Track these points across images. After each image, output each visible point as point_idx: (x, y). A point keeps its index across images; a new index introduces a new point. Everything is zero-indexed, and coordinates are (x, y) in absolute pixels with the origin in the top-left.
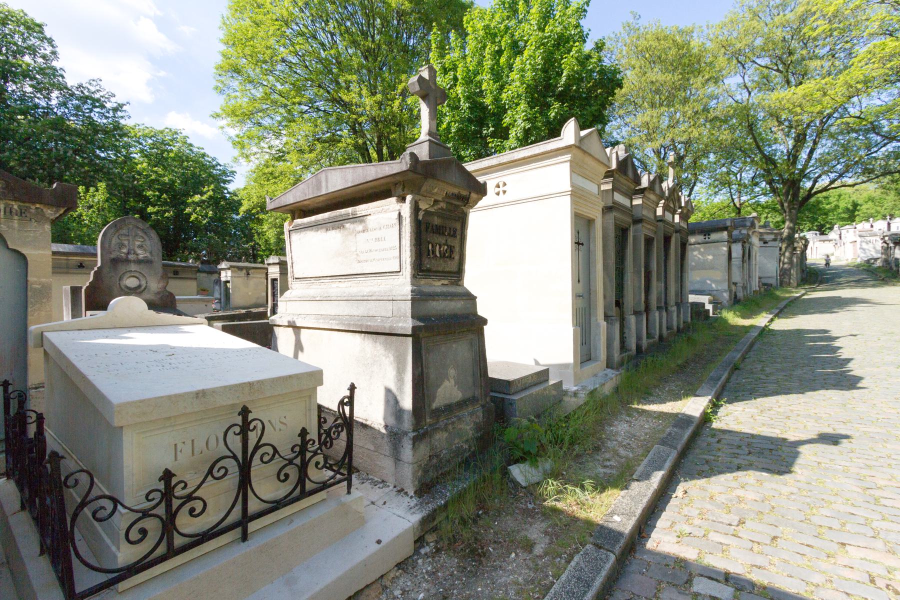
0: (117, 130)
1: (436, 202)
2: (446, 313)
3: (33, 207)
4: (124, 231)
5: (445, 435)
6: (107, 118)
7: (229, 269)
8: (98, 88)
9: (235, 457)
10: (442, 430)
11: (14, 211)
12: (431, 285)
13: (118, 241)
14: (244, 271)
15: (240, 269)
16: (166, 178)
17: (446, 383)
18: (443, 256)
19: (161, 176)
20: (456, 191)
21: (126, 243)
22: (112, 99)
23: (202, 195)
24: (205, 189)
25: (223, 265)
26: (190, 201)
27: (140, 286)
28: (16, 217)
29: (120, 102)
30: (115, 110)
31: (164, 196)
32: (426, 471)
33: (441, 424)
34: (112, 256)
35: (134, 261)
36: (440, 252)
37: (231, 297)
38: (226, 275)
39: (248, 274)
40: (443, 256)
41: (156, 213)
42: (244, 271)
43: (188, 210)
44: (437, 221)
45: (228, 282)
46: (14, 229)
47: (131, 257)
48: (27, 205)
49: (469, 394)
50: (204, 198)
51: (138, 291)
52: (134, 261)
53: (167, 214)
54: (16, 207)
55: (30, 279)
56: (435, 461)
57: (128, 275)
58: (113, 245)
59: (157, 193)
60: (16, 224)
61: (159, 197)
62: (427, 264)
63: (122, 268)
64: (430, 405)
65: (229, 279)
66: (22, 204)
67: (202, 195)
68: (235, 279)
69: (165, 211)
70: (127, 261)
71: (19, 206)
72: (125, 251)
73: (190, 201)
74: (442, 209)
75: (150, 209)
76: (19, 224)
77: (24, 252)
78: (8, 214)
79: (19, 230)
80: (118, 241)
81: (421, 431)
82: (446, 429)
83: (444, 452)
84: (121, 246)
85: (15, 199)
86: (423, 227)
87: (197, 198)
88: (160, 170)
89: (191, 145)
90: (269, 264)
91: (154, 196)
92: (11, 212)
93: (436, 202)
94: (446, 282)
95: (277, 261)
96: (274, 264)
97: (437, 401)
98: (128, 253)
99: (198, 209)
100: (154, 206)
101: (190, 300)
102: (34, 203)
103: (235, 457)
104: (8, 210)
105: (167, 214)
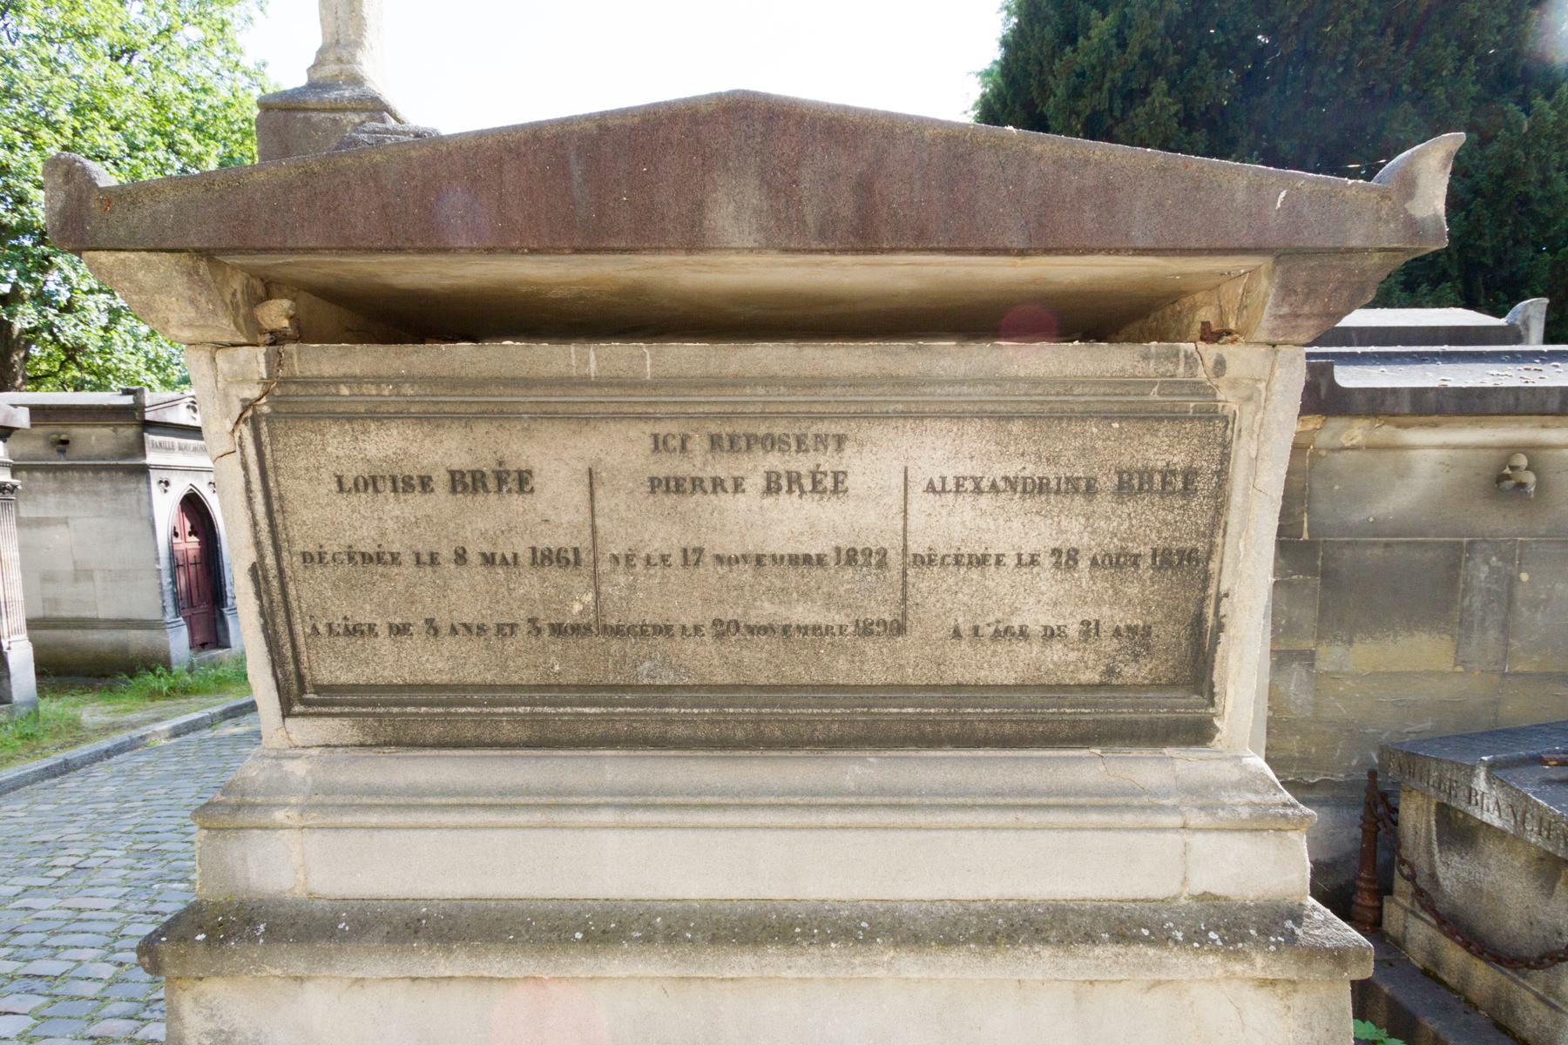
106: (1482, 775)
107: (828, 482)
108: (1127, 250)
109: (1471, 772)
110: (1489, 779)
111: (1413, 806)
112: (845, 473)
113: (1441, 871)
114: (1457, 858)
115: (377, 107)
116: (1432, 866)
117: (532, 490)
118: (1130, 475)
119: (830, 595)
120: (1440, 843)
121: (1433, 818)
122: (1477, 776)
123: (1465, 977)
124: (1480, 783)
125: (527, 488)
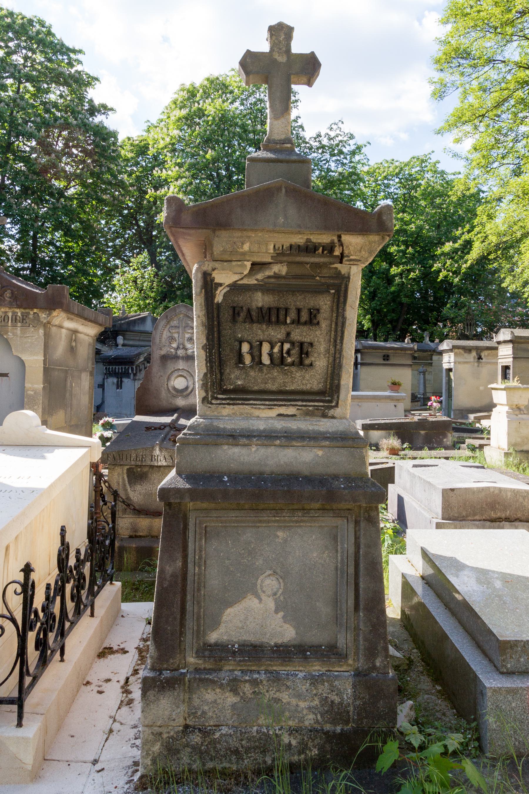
0: (353, 178)
1: (257, 266)
2: (268, 470)
3: (32, 313)
4: (175, 323)
5: (231, 699)
6: (343, 164)
7: (451, 350)
8: (338, 132)
9: (13, 620)
10: (221, 686)
11: (18, 318)
12: (249, 417)
13: (169, 334)
14: (474, 354)
15: (468, 350)
16: (413, 226)
17: (251, 602)
18: (279, 362)
19: (407, 223)
20: (299, 240)
21: (176, 335)
22: (351, 142)
23: (455, 242)
24: (458, 233)
25: (445, 345)
26: (439, 252)
27: (187, 388)
28: (19, 324)
29: (360, 143)
30: (353, 153)
31: (410, 250)
32: (171, 750)
33: (224, 676)
34: (163, 352)
35: (183, 358)
36: (271, 355)
37: (454, 393)
38: (448, 360)
39: (480, 358)
40: (279, 362)
41: (401, 274)
42: (474, 354)
43: (437, 266)
44: (260, 300)
45: (450, 370)
46: (17, 336)
47: (180, 352)
48: (27, 311)
49: (317, 637)
50: (457, 245)
51: (185, 394)
52: (183, 358)
53: (412, 275)
54: (19, 314)
55: (28, 385)
56: (196, 738)
57: (176, 374)
58: (163, 340)
59: (403, 248)
60: (18, 331)
61: (404, 252)
62: (236, 378)
63: (171, 366)
64: (199, 634)
65: (452, 366)
66: (23, 311)
67: (455, 242)
68: (460, 367)
69: (409, 271)
70: (176, 357)
71: (22, 313)
72: (174, 345)
73: (439, 252)
74: (277, 276)
75: (394, 270)
76: (21, 330)
77: (23, 359)
78: (14, 322)
79: (21, 337)
80: (169, 334)
81: (167, 674)
82: (234, 686)
83: (224, 730)
84: (172, 339)
85: (19, 307)
86: (226, 315)
87: (448, 247)
88: (407, 217)
89: (443, 173)
90: (499, 343)
91: (399, 251)
92: (16, 319)
93: (257, 266)
94: (291, 411)
95: (508, 337)
96: (505, 342)
97: (222, 629)
98: (178, 348)
99: (449, 262)
100: (397, 266)
101: (375, 398)
102: (32, 309)
103: (13, 620)
104: (14, 317)
105: (412, 275)
106: (158, 449)
107: (305, 316)
108: (155, 429)
109: (153, 448)
110: (160, 450)
111: (116, 474)
112: (311, 344)
113: (131, 494)
114: (139, 486)
115: (106, 128)
116: (126, 490)
117: (318, 323)
118: (475, 720)
119: (519, 626)
120: (130, 483)
121: (126, 477)
122: (155, 450)
123: (150, 528)
124: (157, 452)
125: (315, 321)
